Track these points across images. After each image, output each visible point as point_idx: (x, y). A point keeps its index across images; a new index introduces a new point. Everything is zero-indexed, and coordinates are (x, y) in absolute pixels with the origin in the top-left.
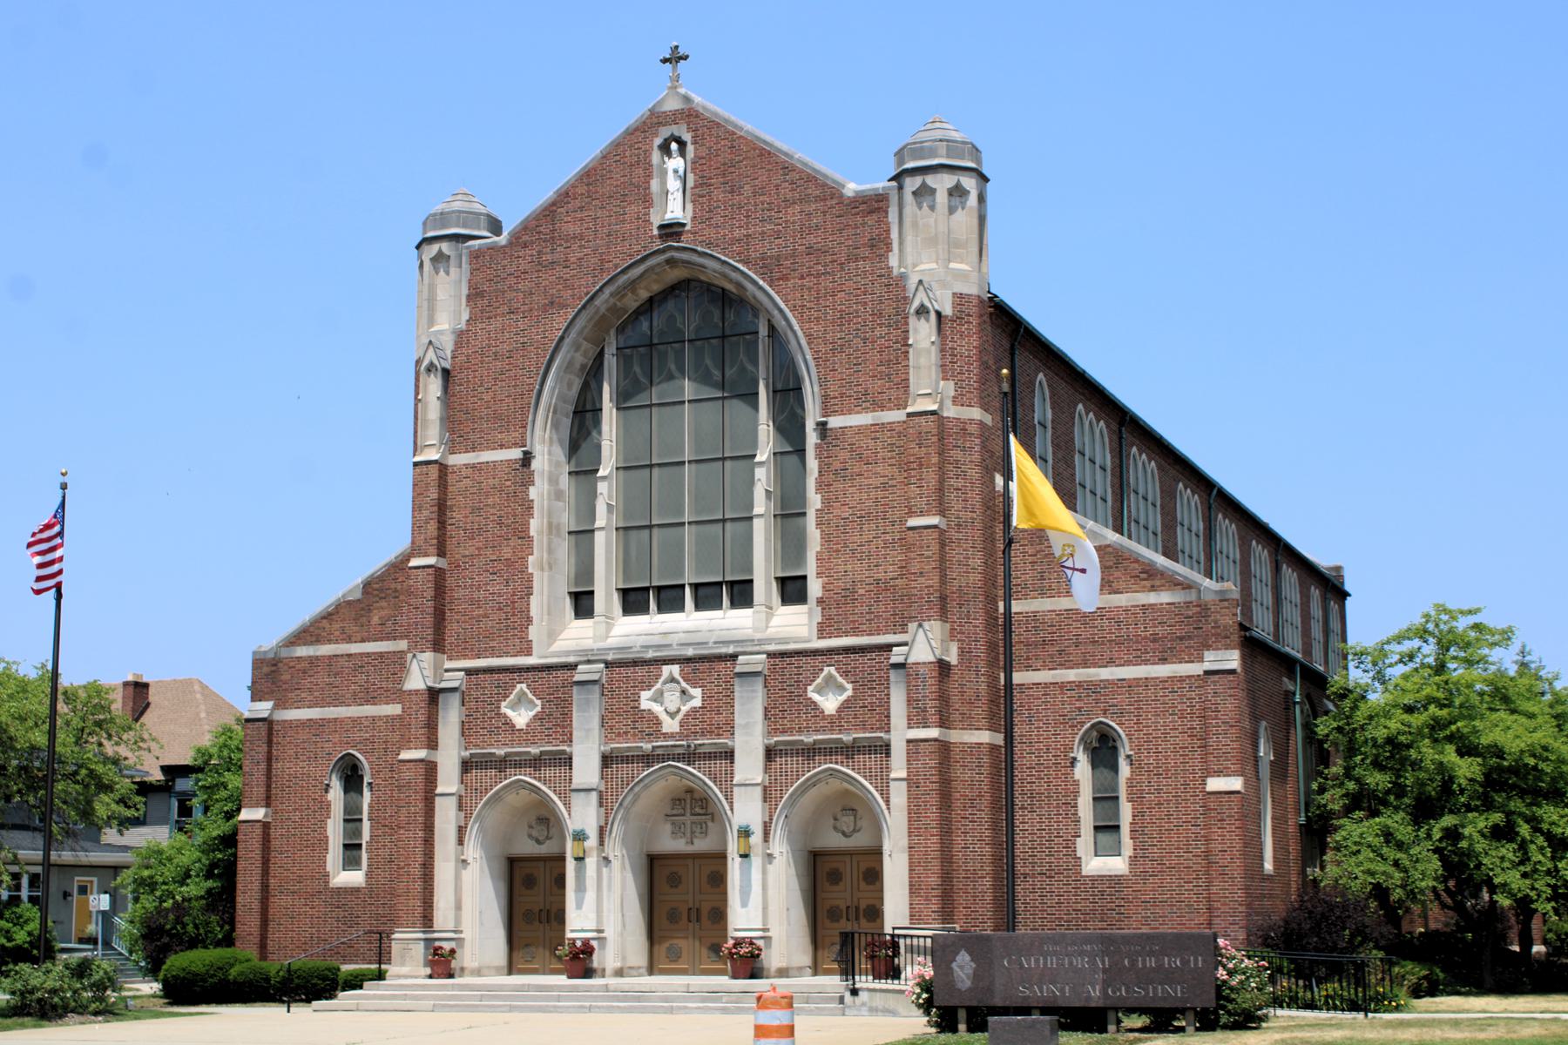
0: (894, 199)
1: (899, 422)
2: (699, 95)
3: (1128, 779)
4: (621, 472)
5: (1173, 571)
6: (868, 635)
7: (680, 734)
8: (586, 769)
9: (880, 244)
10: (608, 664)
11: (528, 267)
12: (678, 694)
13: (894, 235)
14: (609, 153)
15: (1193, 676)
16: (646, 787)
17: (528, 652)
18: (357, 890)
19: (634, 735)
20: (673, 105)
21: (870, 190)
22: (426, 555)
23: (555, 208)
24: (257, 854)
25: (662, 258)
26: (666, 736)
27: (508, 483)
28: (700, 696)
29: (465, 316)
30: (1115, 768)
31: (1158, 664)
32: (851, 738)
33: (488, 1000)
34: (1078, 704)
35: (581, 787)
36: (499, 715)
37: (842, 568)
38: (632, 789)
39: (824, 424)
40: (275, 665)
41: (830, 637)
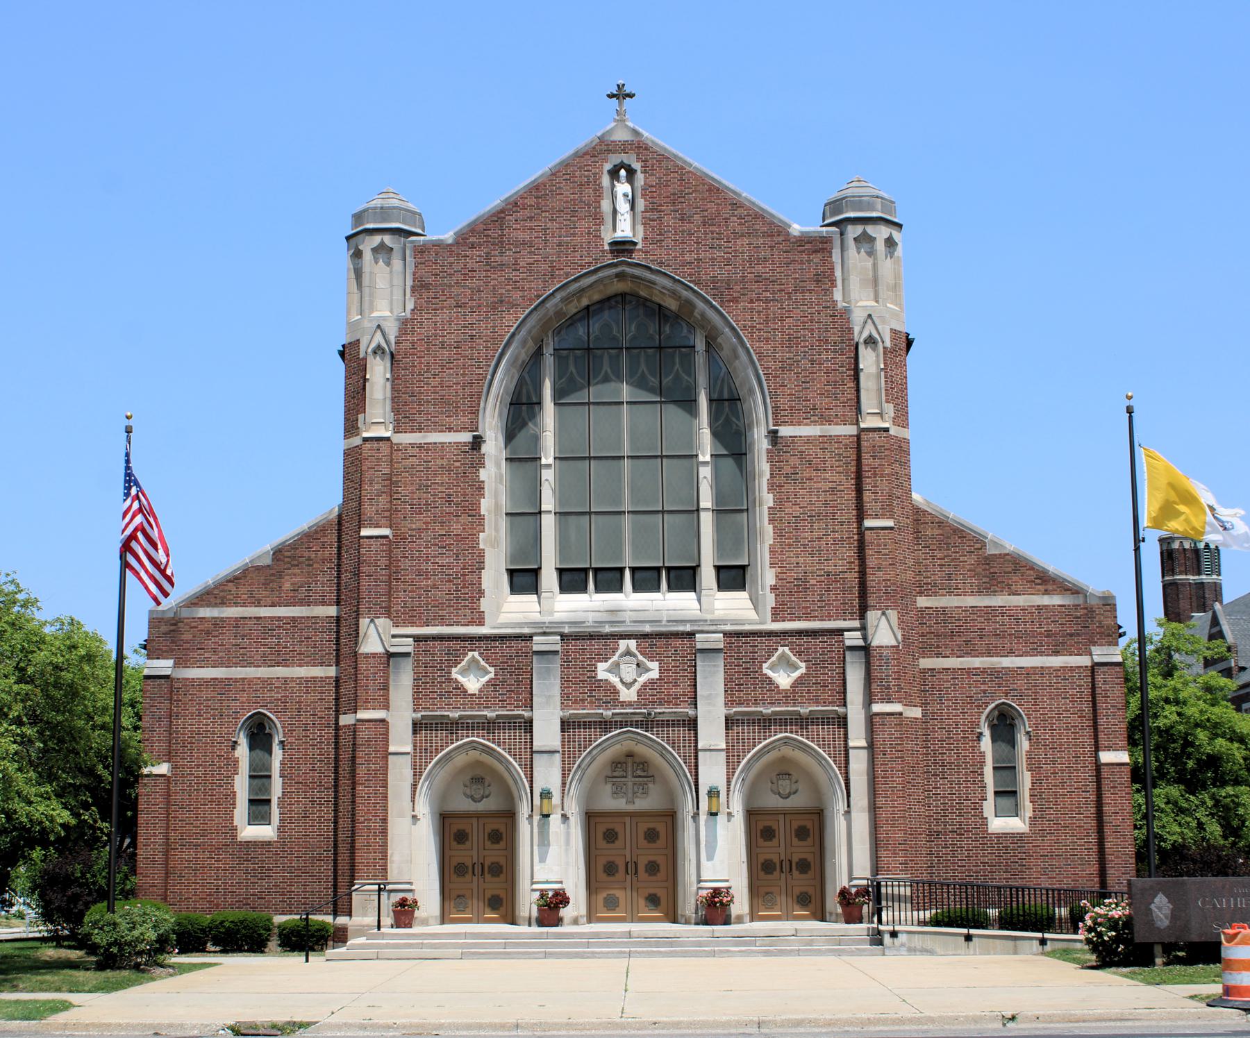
0: (837, 243)
1: (845, 436)
2: (647, 132)
3: (1028, 752)
4: (557, 461)
5: (1063, 578)
6: (819, 620)
7: (638, 702)
8: (547, 732)
9: (825, 280)
10: (563, 637)
11: (476, 266)
12: (635, 666)
13: (838, 273)
14: (559, 171)
15: (1082, 667)
16: (604, 750)
17: (481, 623)
18: (269, 843)
19: (591, 702)
20: (621, 136)
21: (814, 232)
22: (378, 526)
23: (503, 215)
24: (160, 808)
25: (614, 271)
26: (624, 704)
27: (458, 464)
28: (658, 669)
29: (410, 305)
30: (1012, 742)
31: (1051, 655)
32: (808, 711)
33: (585, 948)
34: (983, 687)
35: (543, 749)
36: (450, 680)
37: (794, 560)
38: (590, 752)
39: (776, 432)
40: (175, 625)
41: (784, 621)
